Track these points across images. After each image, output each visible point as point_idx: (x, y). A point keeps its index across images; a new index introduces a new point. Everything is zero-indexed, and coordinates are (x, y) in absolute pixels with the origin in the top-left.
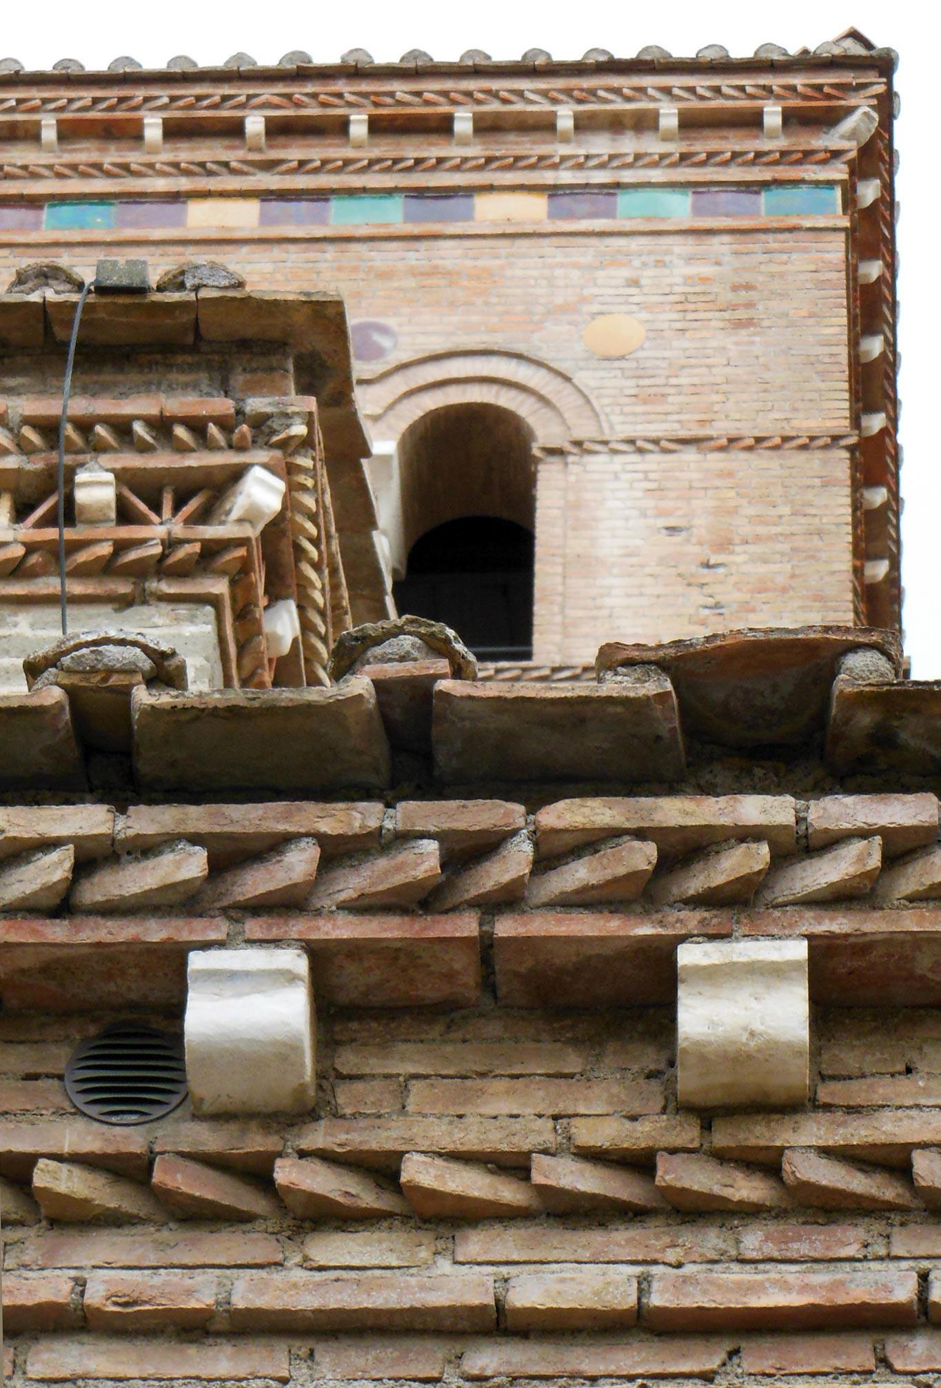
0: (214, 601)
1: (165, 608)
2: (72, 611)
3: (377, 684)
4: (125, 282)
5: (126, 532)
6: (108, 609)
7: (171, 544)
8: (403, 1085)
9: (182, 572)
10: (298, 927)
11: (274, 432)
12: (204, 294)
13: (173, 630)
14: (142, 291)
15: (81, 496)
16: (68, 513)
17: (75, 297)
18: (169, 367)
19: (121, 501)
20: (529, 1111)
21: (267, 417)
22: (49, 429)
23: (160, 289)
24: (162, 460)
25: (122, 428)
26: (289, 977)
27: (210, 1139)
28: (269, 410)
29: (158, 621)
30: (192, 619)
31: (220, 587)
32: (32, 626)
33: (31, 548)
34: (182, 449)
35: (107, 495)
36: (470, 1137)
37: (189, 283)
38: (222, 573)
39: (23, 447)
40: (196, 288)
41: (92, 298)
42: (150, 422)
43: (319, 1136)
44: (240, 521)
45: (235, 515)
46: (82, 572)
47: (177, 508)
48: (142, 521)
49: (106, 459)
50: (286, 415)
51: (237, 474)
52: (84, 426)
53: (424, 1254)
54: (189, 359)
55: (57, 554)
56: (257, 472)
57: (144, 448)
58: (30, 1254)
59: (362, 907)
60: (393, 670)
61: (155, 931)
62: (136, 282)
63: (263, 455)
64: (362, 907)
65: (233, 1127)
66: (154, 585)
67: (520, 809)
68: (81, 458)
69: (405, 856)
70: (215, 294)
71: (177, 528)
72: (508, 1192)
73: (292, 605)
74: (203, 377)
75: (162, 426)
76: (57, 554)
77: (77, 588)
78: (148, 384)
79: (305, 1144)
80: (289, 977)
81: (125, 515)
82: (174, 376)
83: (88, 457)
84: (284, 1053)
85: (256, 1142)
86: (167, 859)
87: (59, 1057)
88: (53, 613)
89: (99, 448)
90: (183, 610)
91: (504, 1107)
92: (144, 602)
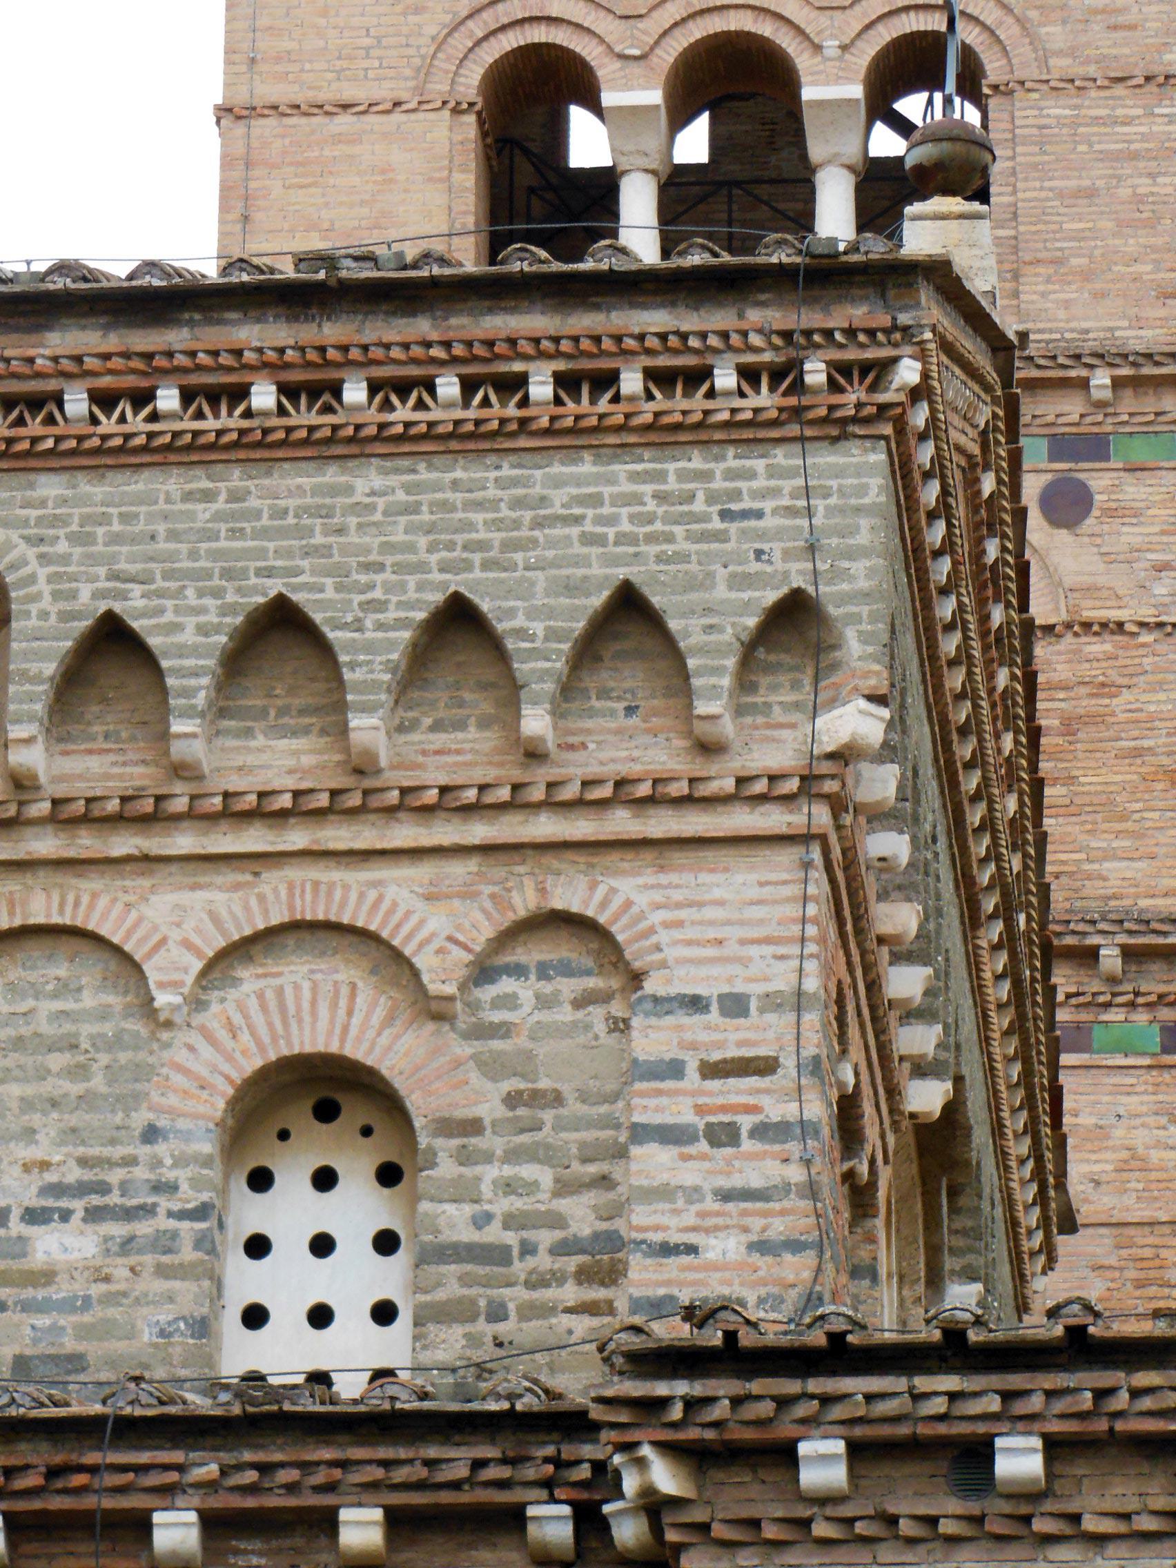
0: (886, 438)
1: (858, 442)
2: (808, 445)
3: (1067, 1328)
4: (826, 252)
5: (836, 399)
6: (826, 443)
7: (859, 405)
8: (1079, 1481)
9: (867, 421)
10: (1037, 1426)
11: (913, 336)
12: (871, 256)
13: (863, 459)
14: (837, 255)
15: (808, 379)
16: (798, 386)
17: (798, 260)
18: (851, 284)
19: (830, 379)
20: (1129, 1493)
21: (910, 327)
22: (787, 335)
23: (845, 253)
24: (851, 354)
25: (828, 334)
26: (1034, 1450)
27: (1007, 1507)
28: (910, 322)
29: (855, 451)
30: (874, 450)
31: (888, 430)
32: (785, 456)
33: (781, 410)
34: (862, 346)
35: (822, 378)
36: (1108, 1506)
37: (862, 249)
38: (889, 419)
39: (776, 348)
40: (867, 253)
41: (808, 260)
42: (843, 331)
43: (1048, 1506)
44: (898, 390)
45: (894, 386)
46: (812, 422)
47: (861, 383)
48: (842, 390)
49: (820, 353)
50: (921, 326)
51: (895, 360)
52: (808, 333)
53: (1091, 1555)
54: (862, 279)
55: (797, 413)
56: (906, 362)
57: (841, 346)
58: (939, 1555)
59: (1062, 1416)
60: (1072, 1321)
61: (981, 1428)
62: (832, 252)
63: (908, 350)
64: (1062, 1416)
65: (1013, 1502)
66: (851, 429)
67: (1122, 1375)
68: (806, 353)
69: (1078, 1397)
70: (878, 257)
71: (863, 396)
72: (1122, 1528)
73: (925, 405)
74: (871, 290)
75: (851, 332)
76: (797, 413)
77: (808, 432)
78: (840, 297)
79: (1043, 1510)
80: (1034, 1450)
81: (834, 386)
82: (856, 292)
83: (810, 352)
84: (1035, 1481)
85: (1024, 1509)
86: (985, 1399)
87: (945, 1464)
88: (797, 448)
89: (818, 346)
90: (868, 444)
91: (1119, 1490)
92: (846, 438)
